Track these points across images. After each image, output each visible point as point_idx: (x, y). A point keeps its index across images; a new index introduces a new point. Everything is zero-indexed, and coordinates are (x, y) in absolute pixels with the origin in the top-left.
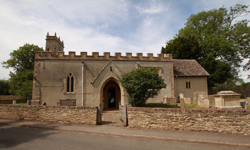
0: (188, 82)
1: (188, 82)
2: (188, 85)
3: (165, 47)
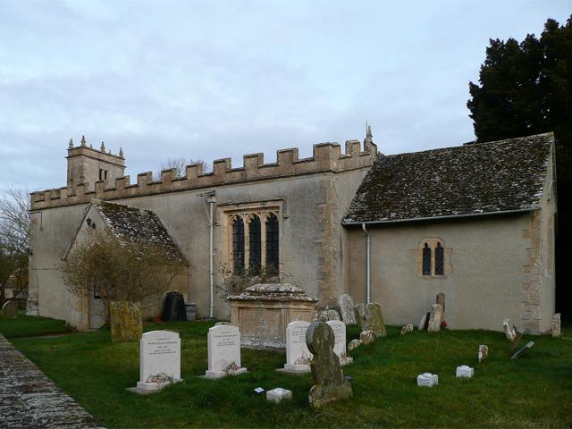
0: (433, 247)
1: (433, 247)
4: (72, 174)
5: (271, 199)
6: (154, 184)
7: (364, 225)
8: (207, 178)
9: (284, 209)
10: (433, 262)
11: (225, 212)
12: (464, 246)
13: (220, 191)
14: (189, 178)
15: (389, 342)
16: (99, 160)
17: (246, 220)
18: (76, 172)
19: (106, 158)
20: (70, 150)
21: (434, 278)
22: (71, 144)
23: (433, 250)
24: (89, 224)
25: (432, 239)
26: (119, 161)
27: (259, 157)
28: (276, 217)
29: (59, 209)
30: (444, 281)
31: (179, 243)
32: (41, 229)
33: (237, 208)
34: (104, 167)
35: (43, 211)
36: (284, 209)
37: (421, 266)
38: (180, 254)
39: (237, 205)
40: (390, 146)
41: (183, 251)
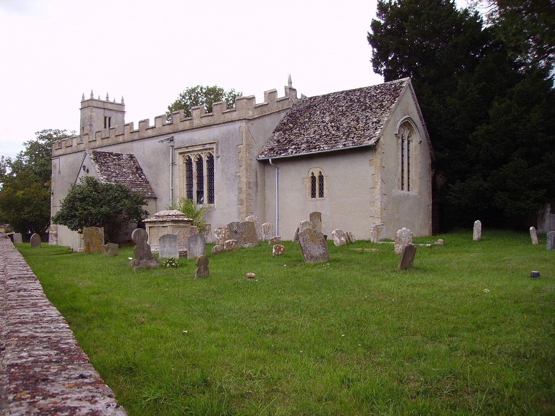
0: (317, 175)
1: (317, 175)
6: (134, 132)
7: (270, 160)
8: (168, 126)
9: (217, 149)
10: (317, 187)
11: (180, 153)
12: (334, 172)
13: (177, 137)
14: (157, 127)
15: (428, 267)
16: (104, 109)
17: (194, 159)
18: (86, 121)
19: (110, 106)
21: (319, 200)
22: (83, 97)
23: (317, 178)
24: (84, 170)
25: (316, 168)
26: (120, 109)
28: (213, 157)
31: (150, 179)
32: (59, 173)
33: (187, 150)
34: (108, 114)
36: (217, 149)
38: (151, 189)
40: (308, 89)
41: (153, 187)
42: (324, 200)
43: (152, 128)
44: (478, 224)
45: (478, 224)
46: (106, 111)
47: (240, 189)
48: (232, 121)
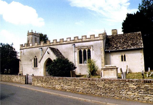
0: (123, 55)
1: (123, 55)
2: (123, 58)
3: (122, 27)
4: (29, 39)
5: (89, 46)
13: (76, 44)
16: (35, 35)
19: (36, 35)
20: (28, 33)
22: (28, 32)
27: (56, 40)
29: (29, 49)
30: (126, 62)
32: (24, 54)
33: (81, 48)
35: (24, 50)
37: (20, 69)
39: (81, 47)
42: (126, 62)
43: (66, 41)
44: (149, 68)
45: (149, 68)
46: (36, 36)
47: (102, 59)
48: (98, 40)
